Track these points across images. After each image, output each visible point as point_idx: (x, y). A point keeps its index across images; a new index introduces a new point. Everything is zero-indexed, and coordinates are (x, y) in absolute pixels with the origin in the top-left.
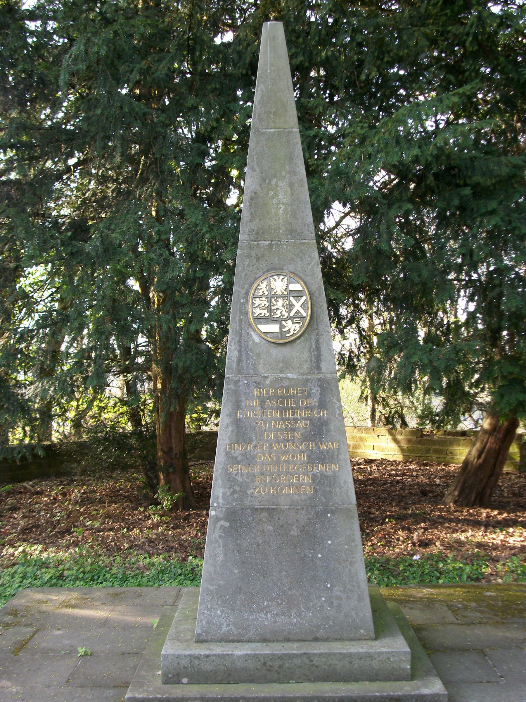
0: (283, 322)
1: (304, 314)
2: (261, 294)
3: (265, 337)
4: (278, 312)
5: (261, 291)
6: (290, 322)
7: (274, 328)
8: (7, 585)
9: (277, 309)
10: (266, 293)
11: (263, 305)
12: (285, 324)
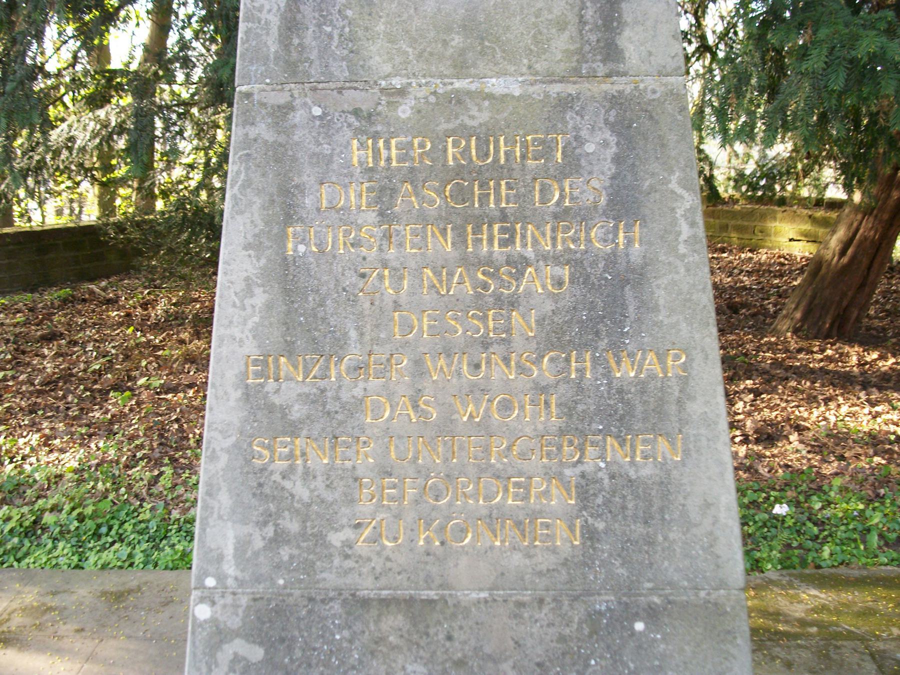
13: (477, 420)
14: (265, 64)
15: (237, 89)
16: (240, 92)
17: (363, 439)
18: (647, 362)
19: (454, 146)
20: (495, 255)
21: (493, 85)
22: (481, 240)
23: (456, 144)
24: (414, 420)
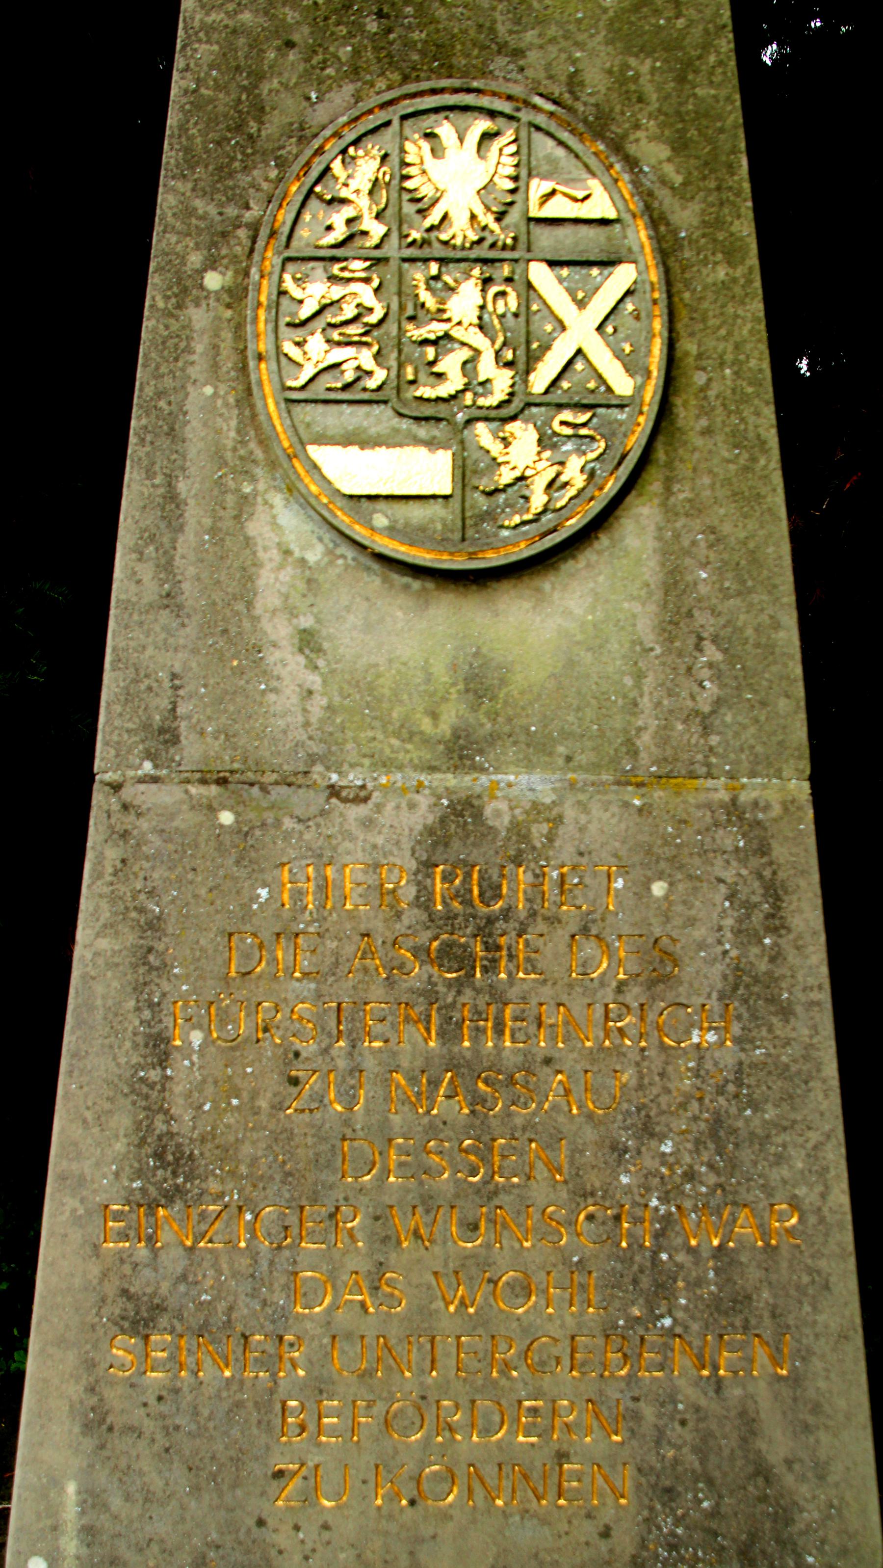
0: (483, 433)
1: (623, 384)
2: (340, 233)
3: (360, 532)
4: (451, 363)
5: (339, 218)
6: (524, 435)
7: (428, 470)
8: (328, 133)
9: (443, 342)
10: (377, 230)
11: (349, 312)
12: (496, 449)
13: (471, 1310)
14: (509, 1115)
15: (97, 777)
16: (101, 782)
17: (288, 1338)
18: (739, 1222)
19: (444, 879)
20: (505, 1054)
21: (510, 785)
22: (484, 1031)
23: (447, 878)
24: (371, 1310)
